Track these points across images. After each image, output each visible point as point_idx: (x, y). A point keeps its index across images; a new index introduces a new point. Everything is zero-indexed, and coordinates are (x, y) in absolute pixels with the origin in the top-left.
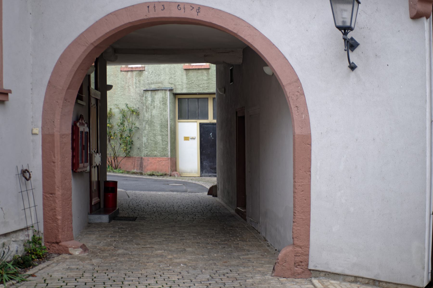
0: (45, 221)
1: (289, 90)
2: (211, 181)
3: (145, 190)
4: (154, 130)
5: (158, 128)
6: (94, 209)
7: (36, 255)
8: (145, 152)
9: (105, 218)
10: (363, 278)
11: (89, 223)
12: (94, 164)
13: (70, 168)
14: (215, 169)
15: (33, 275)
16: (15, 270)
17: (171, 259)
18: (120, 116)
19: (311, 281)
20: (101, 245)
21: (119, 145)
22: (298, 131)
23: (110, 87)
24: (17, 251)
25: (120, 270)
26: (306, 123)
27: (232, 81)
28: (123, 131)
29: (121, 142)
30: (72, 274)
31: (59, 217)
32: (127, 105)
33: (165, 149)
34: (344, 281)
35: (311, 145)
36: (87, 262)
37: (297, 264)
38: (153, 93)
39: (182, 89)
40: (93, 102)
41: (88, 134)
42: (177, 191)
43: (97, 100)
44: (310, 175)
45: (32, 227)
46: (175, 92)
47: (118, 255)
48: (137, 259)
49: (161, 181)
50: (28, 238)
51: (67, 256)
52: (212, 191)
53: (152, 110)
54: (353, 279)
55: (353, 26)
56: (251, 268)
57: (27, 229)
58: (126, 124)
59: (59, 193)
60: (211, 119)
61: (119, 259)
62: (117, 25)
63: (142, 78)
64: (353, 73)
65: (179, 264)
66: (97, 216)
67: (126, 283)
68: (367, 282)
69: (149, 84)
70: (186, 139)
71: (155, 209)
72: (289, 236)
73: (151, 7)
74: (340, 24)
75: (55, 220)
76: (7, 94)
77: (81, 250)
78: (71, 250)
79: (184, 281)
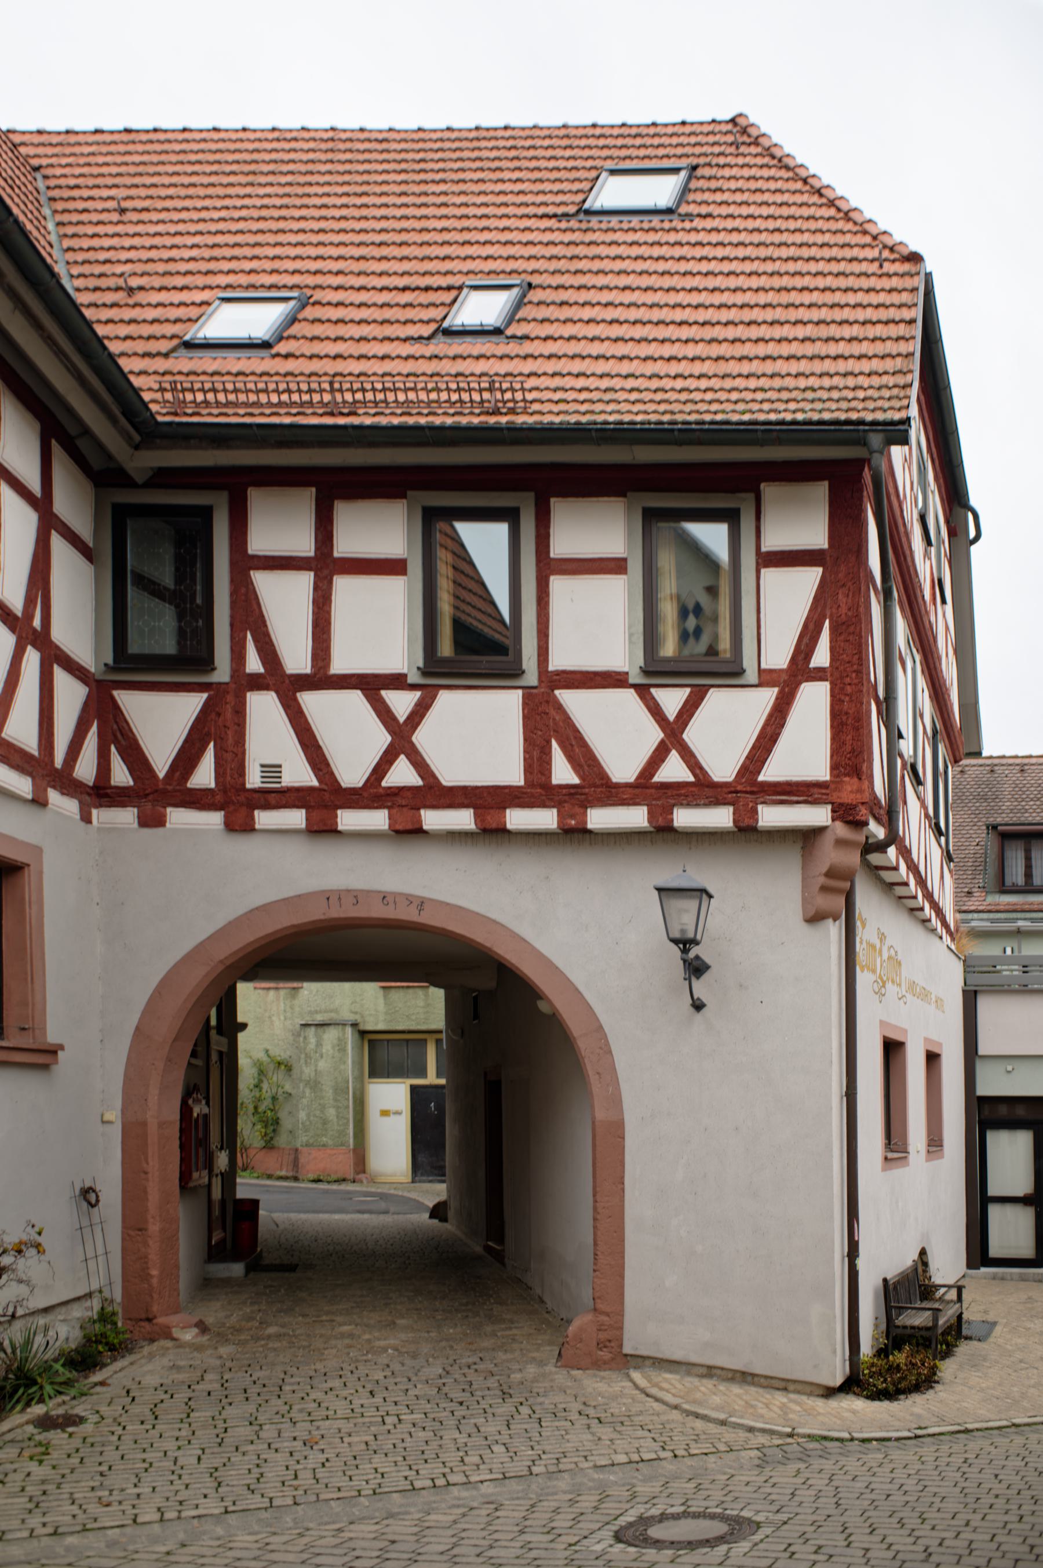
0: (125, 1280)
1: (584, 1045)
2: (435, 1192)
3: (308, 1212)
4: (322, 1098)
5: (329, 1093)
6: (215, 1253)
7: (107, 1344)
8: (302, 1139)
9: (237, 1269)
10: (722, 1369)
11: (206, 1279)
12: (216, 1171)
13: (177, 1181)
14: (443, 1167)
15: (102, 1383)
16: (68, 1375)
17: (369, 1341)
18: (254, 1071)
19: (628, 1376)
20: (234, 1319)
21: (250, 1125)
22: (600, 1114)
23: (244, 1026)
24: (67, 1339)
25: (273, 1364)
26: (616, 1101)
27: (476, 1016)
28: (259, 1099)
29: (255, 1119)
30: (181, 1377)
31: (154, 1272)
32: (267, 1051)
33: (342, 1133)
34: (689, 1373)
35: (623, 1138)
36: (209, 1352)
37: (601, 1345)
38: (320, 1030)
39: (376, 1022)
40: (214, 1057)
41: (206, 1117)
42: (370, 1212)
43: (221, 1053)
44: (623, 1190)
45: (100, 1292)
46: (362, 1027)
47: (269, 1337)
48: (305, 1343)
49: (335, 1192)
50: (89, 1314)
51: (169, 1344)
52: (438, 1212)
53: (316, 1060)
54: (704, 1371)
55: (699, 937)
56: (517, 1353)
57: (89, 1295)
58: (265, 1086)
59: (154, 1228)
60: (432, 1078)
61: (271, 1345)
62: (270, 930)
63: (296, 1002)
64: (699, 1017)
65: (385, 1350)
66: (221, 1266)
67: (287, 1388)
68: (730, 1375)
69: (310, 1012)
70: (385, 1113)
71: (331, 1248)
72: (586, 1294)
73: (334, 900)
74: (677, 935)
75: (146, 1277)
76: (55, 1053)
77: (195, 1330)
78: (176, 1333)
79: (397, 1380)
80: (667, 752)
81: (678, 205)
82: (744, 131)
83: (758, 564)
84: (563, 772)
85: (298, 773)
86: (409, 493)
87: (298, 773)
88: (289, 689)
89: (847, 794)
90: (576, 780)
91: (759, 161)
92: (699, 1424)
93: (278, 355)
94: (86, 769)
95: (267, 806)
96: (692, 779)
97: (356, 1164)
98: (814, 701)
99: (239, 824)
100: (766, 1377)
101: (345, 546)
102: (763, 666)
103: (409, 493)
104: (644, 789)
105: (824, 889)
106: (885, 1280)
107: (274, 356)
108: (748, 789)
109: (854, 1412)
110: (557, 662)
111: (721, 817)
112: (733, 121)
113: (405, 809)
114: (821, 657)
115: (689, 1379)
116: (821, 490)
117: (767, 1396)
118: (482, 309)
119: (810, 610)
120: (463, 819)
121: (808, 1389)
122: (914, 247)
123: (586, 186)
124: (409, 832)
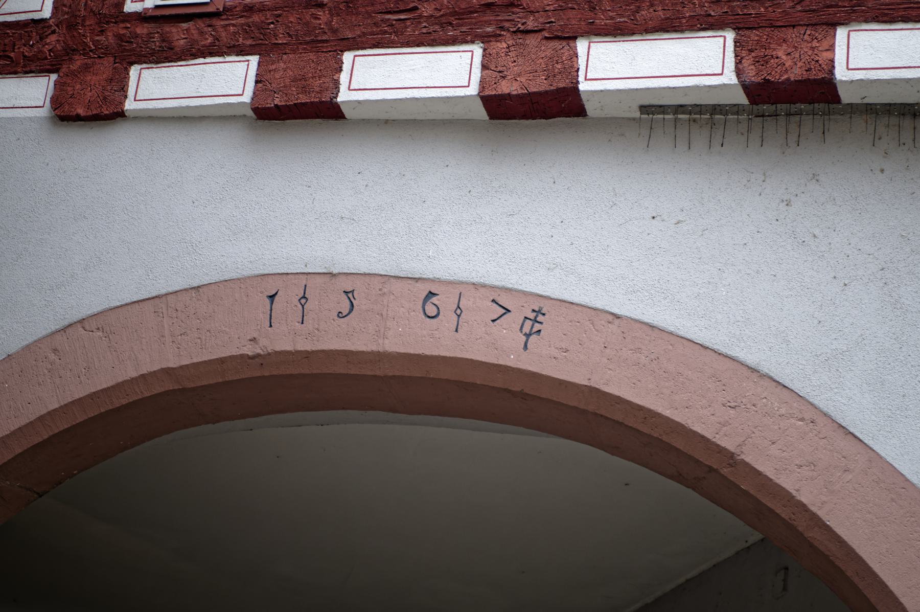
95: (166, 55)
113: (532, 41)
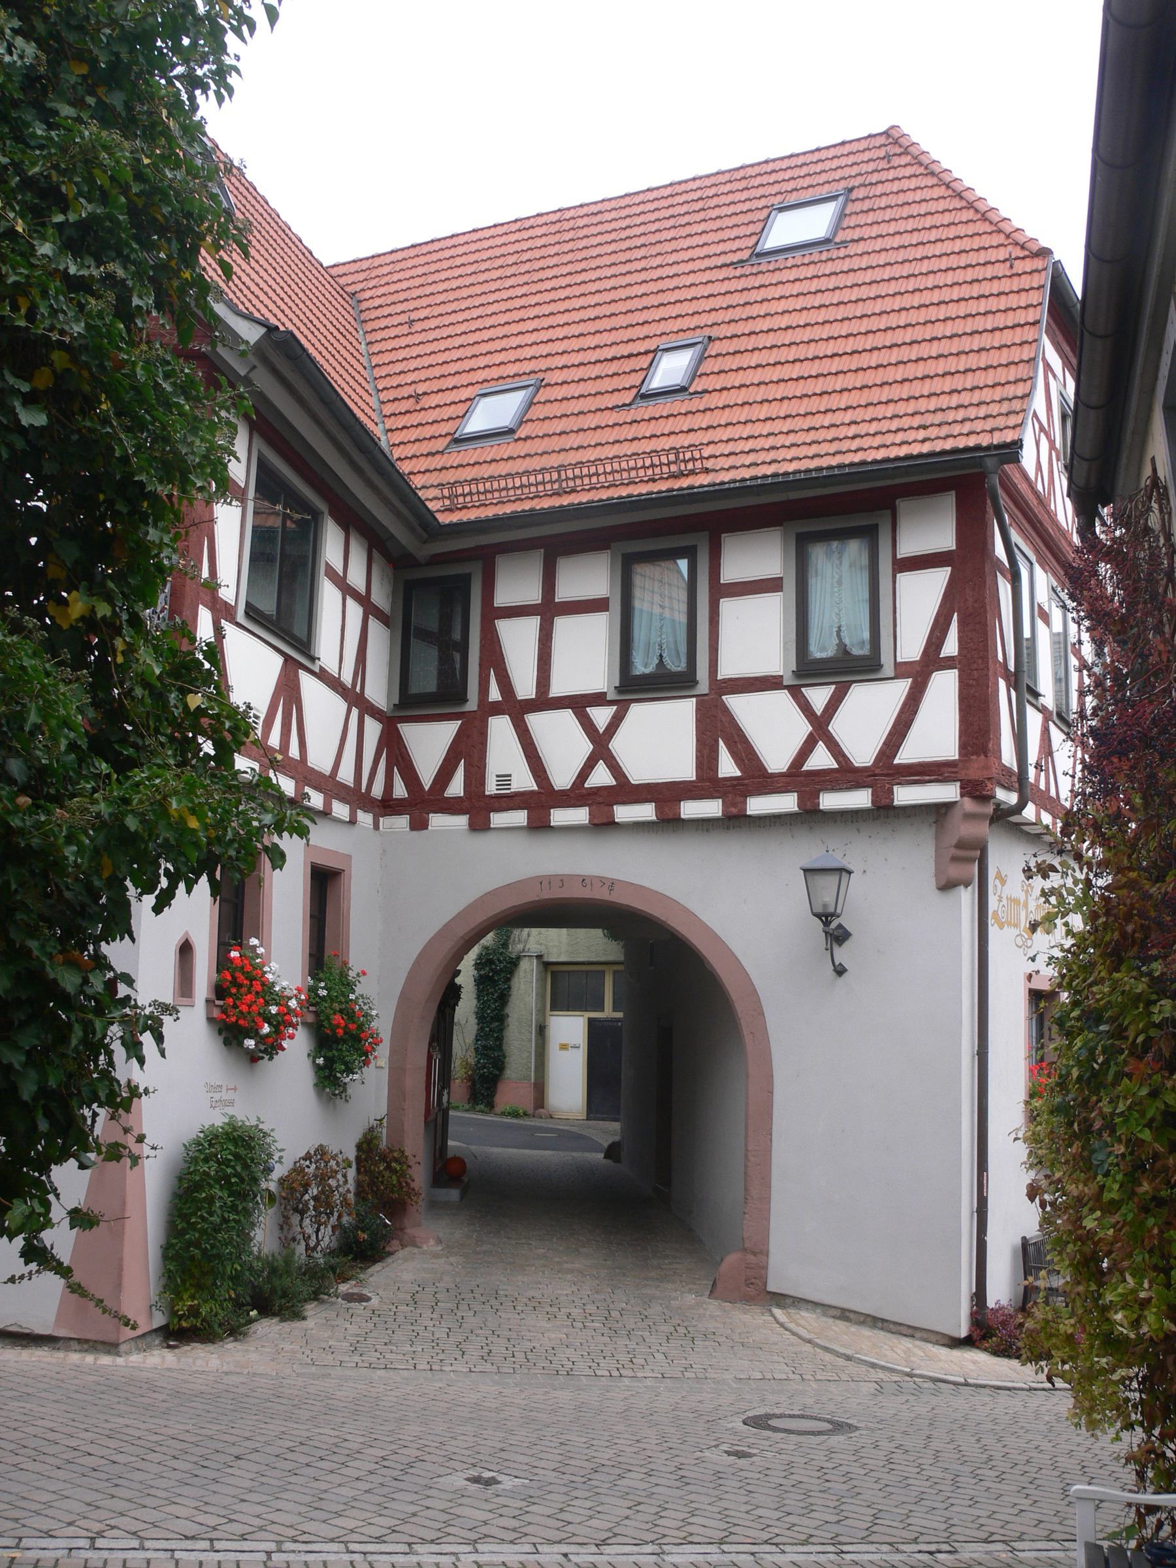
2: (610, 1131)
10: (855, 1312)
34: (825, 1315)
46: (545, 959)
52: (612, 1152)
60: (608, 1012)
70: (564, 1047)
73: (545, 883)
74: (819, 910)
80: (815, 743)
81: (835, 234)
82: (896, 142)
83: (894, 570)
84: (728, 767)
85: (523, 781)
86: (613, 544)
87: (523, 781)
88: (518, 710)
89: (974, 771)
90: (739, 774)
91: (908, 171)
92: (828, 1357)
93: (520, 439)
94: (378, 791)
96: (836, 766)
97: (536, 1099)
98: (944, 687)
99: (480, 825)
100: (895, 1323)
101: (565, 591)
102: (899, 660)
103: (613, 544)
104: (796, 777)
105: (955, 859)
106: (1024, 1238)
107: (516, 440)
108: (886, 771)
109: (974, 1362)
110: (728, 669)
111: (861, 799)
112: (886, 133)
114: (951, 647)
115: (824, 1319)
116: (949, 501)
117: (894, 1340)
118: (672, 369)
119: (941, 606)
120: (646, 812)
121: (933, 1338)
122: (1044, 243)
123: (757, 228)
124: (604, 824)
